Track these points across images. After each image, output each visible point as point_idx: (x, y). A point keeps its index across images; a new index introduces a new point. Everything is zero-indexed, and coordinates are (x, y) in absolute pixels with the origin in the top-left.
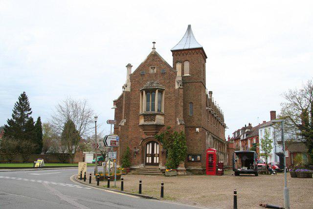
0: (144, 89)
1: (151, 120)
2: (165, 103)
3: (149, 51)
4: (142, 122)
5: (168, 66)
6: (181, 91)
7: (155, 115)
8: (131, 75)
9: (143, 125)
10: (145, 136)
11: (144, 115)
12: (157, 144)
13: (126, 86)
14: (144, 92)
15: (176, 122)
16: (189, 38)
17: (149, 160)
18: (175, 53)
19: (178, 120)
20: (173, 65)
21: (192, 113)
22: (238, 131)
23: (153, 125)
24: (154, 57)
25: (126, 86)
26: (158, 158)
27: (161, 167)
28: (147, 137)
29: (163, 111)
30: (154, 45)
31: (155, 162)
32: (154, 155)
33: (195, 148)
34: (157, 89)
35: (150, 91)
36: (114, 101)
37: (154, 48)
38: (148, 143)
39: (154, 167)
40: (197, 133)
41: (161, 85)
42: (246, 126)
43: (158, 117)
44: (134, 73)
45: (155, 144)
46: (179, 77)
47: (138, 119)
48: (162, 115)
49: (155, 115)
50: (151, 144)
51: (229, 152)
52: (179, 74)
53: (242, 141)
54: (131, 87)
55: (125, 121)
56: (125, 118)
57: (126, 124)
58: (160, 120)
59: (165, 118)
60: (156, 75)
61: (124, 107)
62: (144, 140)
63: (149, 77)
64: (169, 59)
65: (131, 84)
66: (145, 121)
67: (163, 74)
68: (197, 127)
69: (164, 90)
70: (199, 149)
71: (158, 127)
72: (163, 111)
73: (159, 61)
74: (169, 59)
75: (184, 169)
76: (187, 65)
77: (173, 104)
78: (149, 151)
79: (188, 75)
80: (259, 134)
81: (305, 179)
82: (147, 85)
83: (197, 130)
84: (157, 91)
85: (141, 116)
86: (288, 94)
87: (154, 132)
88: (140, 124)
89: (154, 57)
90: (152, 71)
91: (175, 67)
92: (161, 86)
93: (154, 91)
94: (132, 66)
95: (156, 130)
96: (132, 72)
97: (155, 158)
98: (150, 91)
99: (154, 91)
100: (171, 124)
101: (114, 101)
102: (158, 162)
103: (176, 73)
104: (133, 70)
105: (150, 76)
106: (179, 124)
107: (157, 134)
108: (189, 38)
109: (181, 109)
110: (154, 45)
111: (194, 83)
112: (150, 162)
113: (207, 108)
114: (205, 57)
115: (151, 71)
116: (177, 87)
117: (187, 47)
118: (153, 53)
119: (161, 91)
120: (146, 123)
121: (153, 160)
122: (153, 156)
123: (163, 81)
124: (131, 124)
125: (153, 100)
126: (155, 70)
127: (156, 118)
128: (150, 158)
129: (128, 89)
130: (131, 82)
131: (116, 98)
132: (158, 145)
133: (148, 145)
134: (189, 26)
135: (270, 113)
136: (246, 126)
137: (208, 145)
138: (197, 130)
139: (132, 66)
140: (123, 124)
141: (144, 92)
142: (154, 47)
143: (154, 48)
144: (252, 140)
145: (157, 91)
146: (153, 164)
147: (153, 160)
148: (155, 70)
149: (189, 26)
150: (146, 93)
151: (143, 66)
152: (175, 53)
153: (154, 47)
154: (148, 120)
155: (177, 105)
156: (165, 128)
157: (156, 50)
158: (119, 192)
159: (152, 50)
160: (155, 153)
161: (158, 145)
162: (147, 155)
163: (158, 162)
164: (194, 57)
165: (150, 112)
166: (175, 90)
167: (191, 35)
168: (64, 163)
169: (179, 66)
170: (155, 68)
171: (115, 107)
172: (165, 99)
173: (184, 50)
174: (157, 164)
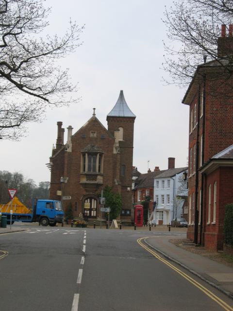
1: (93, 180)
3: (90, 116)
4: (84, 180)
5: (105, 129)
7: (97, 175)
8: (72, 137)
10: (85, 193)
11: (86, 175)
12: (95, 199)
14: (87, 155)
26: (95, 212)
28: (87, 193)
31: (92, 215)
35: (92, 154)
37: (94, 114)
38: (87, 199)
39: (93, 219)
40: (128, 191)
41: (101, 149)
43: (99, 177)
45: (93, 200)
48: (102, 175)
49: (97, 175)
50: (89, 200)
54: (72, 148)
55: (68, 178)
57: (68, 181)
58: (100, 180)
59: (104, 178)
60: (96, 139)
61: (66, 166)
62: (84, 196)
64: (105, 124)
65: (73, 145)
66: (87, 180)
67: (103, 139)
68: (128, 187)
74: (105, 124)
78: (87, 205)
80: (155, 185)
88: (81, 182)
89: (94, 122)
92: (100, 151)
93: (96, 154)
94: (73, 128)
96: (73, 134)
97: (92, 212)
98: (92, 154)
99: (96, 154)
102: (95, 215)
105: (91, 139)
106: (117, 184)
115: (91, 135)
116: (115, 152)
122: (91, 210)
125: (95, 162)
126: (95, 135)
130: (73, 143)
133: (86, 201)
134: (122, 92)
135: (168, 160)
136: (171, 161)
139: (73, 128)
141: (87, 155)
142: (94, 113)
143: (94, 114)
144: (143, 192)
147: (90, 213)
148: (95, 135)
149: (122, 92)
150: (88, 155)
151: (83, 131)
152: (109, 118)
153: (94, 113)
154: (90, 180)
157: (96, 116)
159: (92, 116)
160: (93, 207)
161: (95, 201)
162: (85, 209)
163: (95, 215)
165: (92, 172)
167: (124, 102)
170: (95, 132)
172: (104, 161)
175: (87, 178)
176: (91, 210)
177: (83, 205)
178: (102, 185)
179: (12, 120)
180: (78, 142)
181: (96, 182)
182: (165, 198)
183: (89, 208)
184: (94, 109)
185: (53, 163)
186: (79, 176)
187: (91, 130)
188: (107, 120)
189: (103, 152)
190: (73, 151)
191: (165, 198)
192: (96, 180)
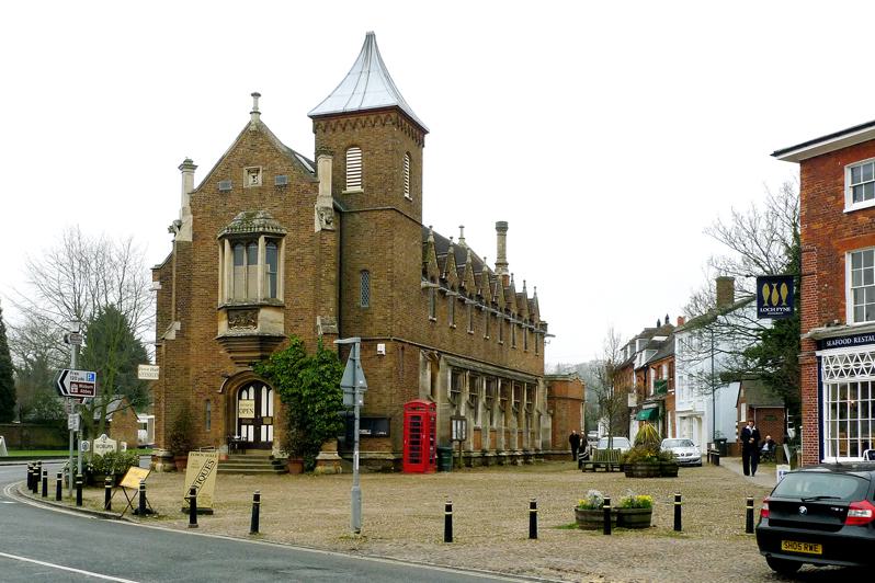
0: (224, 236)
1: (247, 323)
2: (286, 273)
3: (241, 121)
4: (223, 329)
6: (331, 241)
7: (255, 308)
9: (225, 338)
10: (232, 369)
11: (229, 310)
13: (179, 227)
14: (227, 242)
15: (316, 328)
16: (364, 76)
17: (248, 433)
18: (322, 122)
19: (319, 323)
20: (203, 183)
21: (366, 298)
22: (632, 343)
23: (251, 336)
24: (255, 139)
25: (179, 227)
27: (276, 452)
28: (240, 370)
29: (280, 297)
30: (256, 103)
31: (263, 439)
32: (262, 418)
33: (375, 400)
34: (263, 233)
36: (154, 270)
37: (256, 112)
38: (246, 387)
42: (659, 324)
43: (263, 313)
44: (201, 185)
45: (264, 390)
46: (325, 200)
47: (215, 321)
48: (279, 307)
49: (255, 308)
50: (252, 390)
51: (554, 408)
52: (325, 187)
53: (638, 371)
54: (194, 227)
55: (177, 325)
56: (176, 320)
57: (179, 334)
58: (270, 322)
61: (174, 284)
62: (230, 378)
63: (241, 199)
64: (302, 142)
66: (230, 326)
69: (284, 235)
70: (384, 402)
71: (266, 342)
72: (280, 297)
73: (268, 150)
74: (302, 142)
75: (336, 456)
76: (354, 158)
77: (308, 275)
78: (246, 407)
79: (358, 189)
81: (658, 479)
82: (236, 222)
83: (381, 347)
84: (262, 240)
85: (220, 312)
86: (730, 224)
87: (254, 358)
88: (220, 334)
89: (255, 139)
90: (251, 180)
91: (315, 165)
92: (275, 226)
95: (261, 350)
96: (197, 184)
97: (264, 428)
100: (303, 334)
101: (154, 270)
103: (315, 184)
104: (199, 177)
105: (246, 194)
107: (264, 362)
108: (364, 76)
109: (330, 291)
110: (256, 103)
111: (374, 214)
112: (251, 439)
113: (423, 284)
114: (417, 132)
117: (354, 106)
118: (253, 128)
119: (274, 240)
120: (235, 332)
121: (257, 433)
122: (257, 422)
123: (280, 209)
124: (196, 334)
126: (260, 177)
127: (259, 317)
128: (251, 428)
129: (186, 235)
130: (194, 213)
131: (161, 260)
132: (271, 393)
133: (244, 394)
134: (370, 37)
136: (659, 324)
137: (425, 390)
138: (381, 347)
140: (172, 336)
141: (227, 242)
142: (256, 107)
143: (256, 112)
145: (262, 240)
146: (257, 444)
147: (257, 433)
148: (260, 177)
149: (370, 37)
152: (322, 122)
153: (256, 107)
155: (317, 284)
156: (288, 344)
157: (262, 118)
158: (72, 509)
159: (248, 118)
160: (264, 414)
162: (241, 422)
163: (271, 439)
164: (392, 133)
165: (242, 298)
166: (313, 235)
168: (29, 448)
169: (326, 166)
170: (258, 171)
171: (157, 285)
172: (286, 261)
173: (345, 114)
174: (268, 445)
175: (229, 319)
176: (257, 422)
177: (231, 408)
178: (281, 338)
179: (406, 346)
180: (208, 207)
181: (256, 331)
182: (52, 492)
183: (253, 416)
184: (462, 227)
185: (161, 283)
186: (213, 313)
187: (247, 164)
188: (315, 132)
189: (284, 232)
190: (195, 236)
191: (52, 492)
192: (255, 324)
